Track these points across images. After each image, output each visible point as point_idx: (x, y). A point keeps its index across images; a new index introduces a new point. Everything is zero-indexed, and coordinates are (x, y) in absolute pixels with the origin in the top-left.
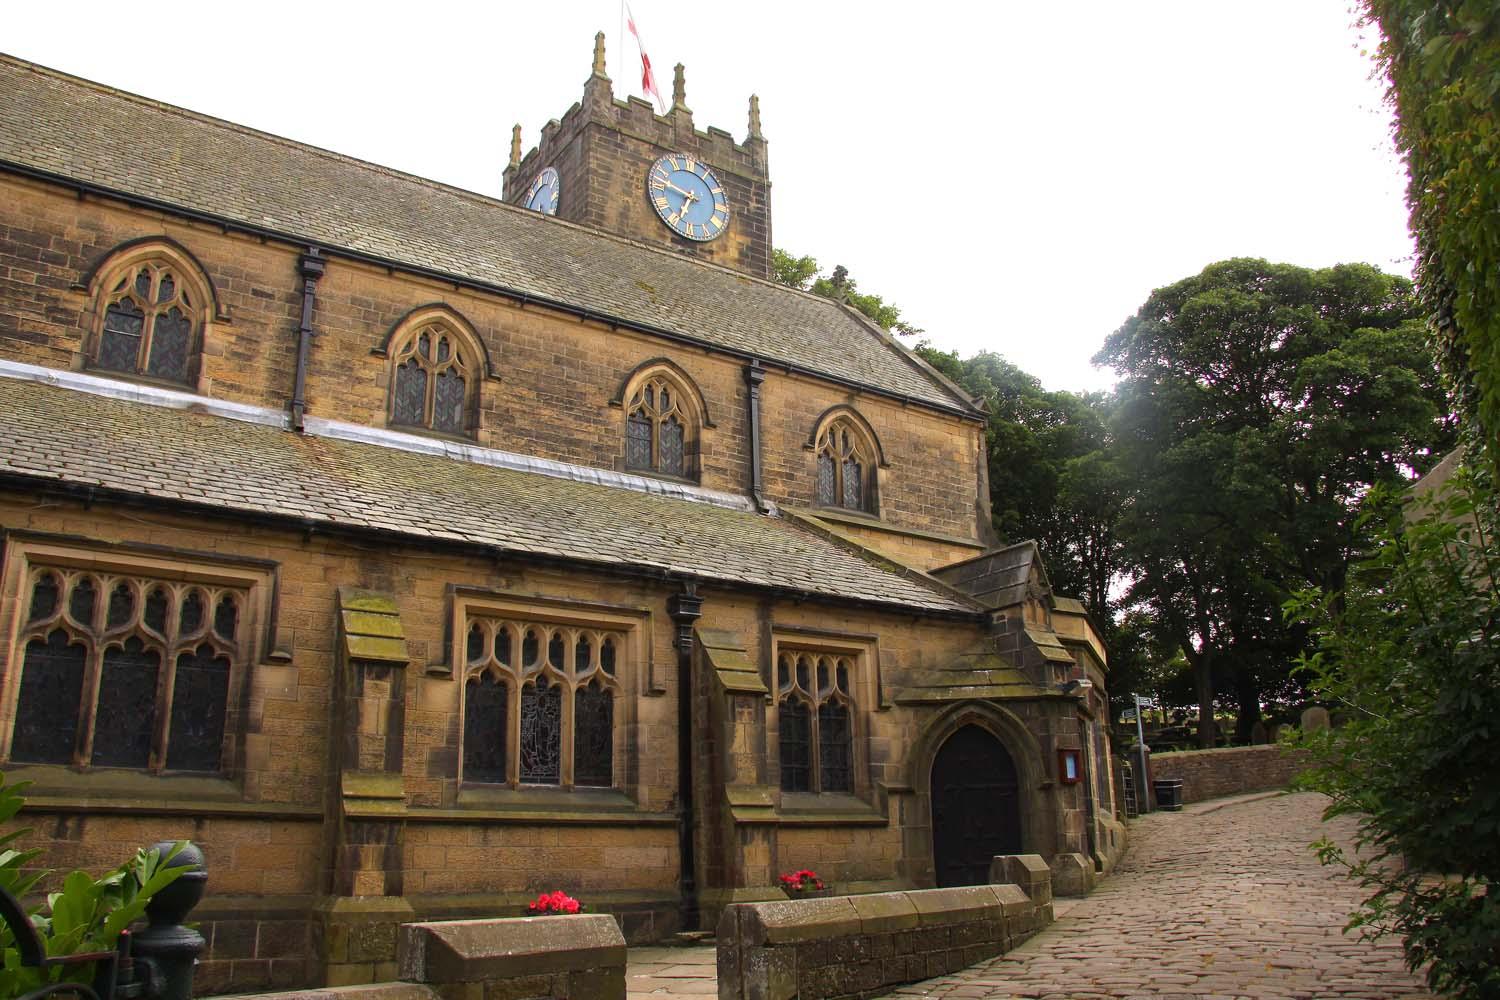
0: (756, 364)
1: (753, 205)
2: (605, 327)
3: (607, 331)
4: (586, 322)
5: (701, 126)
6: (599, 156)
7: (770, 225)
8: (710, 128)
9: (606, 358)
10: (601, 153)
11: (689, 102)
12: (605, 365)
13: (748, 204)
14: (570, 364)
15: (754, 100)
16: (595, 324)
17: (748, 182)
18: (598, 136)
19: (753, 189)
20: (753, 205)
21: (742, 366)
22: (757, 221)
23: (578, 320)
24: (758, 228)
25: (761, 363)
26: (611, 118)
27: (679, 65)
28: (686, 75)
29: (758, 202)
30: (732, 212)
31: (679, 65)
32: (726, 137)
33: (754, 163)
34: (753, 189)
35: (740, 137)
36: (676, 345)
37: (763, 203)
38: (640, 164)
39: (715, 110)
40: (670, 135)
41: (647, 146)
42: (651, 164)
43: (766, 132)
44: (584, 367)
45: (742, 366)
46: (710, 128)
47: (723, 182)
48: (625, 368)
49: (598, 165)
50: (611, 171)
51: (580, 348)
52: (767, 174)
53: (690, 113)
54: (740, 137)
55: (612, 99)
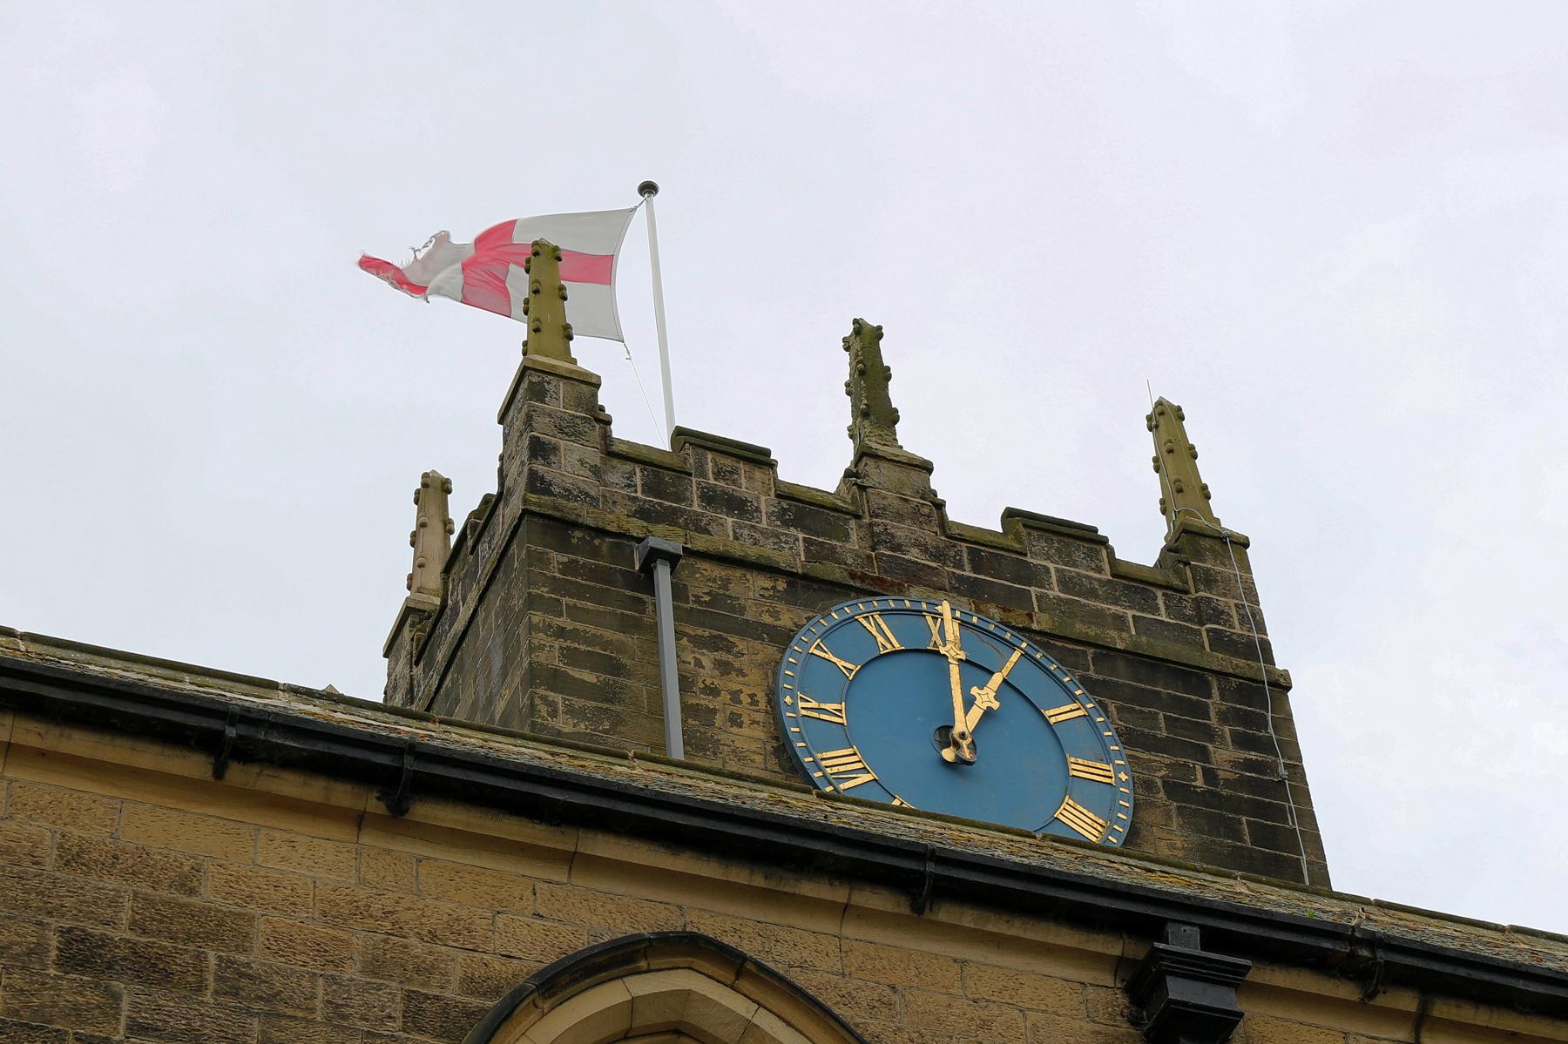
0: (1184, 940)
1: (1224, 755)
2: (343, 795)
3: (360, 821)
4: (237, 774)
5: (973, 505)
6: (564, 621)
7: (1309, 817)
8: (1010, 515)
9: (359, 940)
10: (574, 613)
11: (910, 438)
12: (352, 972)
13: (1204, 754)
14: (150, 969)
15: (1166, 419)
16: (289, 785)
17: (1193, 677)
18: (557, 558)
19: (1215, 702)
20: (1224, 755)
21: (1119, 964)
22: (1257, 809)
23: (194, 765)
24: (1260, 835)
25: (1211, 939)
26: (618, 503)
27: (859, 326)
28: (889, 352)
29: (1242, 742)
30: (1143, 785)
31: (859, 326)
32: (1087, 539)
33: (1207, 612)
34: (1215, 702)
35: (1140, 540)
36: (739, 875)
37: (1265, 746)
38: (741, 644)
39: (1012, 445)
40: (854, 542)
41: (763, 582)
42: (783, 639)
43: (1228, 513)
44: (235, 981)
45: (1119, 965)
46: (1010, 515)
47: (1086, 683)
48: (471, 985)
49: (571, 656)
50: (616, 669)
51: (209, 895)
52: (1266, 647)
53: (927, 468)
54: (1140, 540)
55: (606, 436)
